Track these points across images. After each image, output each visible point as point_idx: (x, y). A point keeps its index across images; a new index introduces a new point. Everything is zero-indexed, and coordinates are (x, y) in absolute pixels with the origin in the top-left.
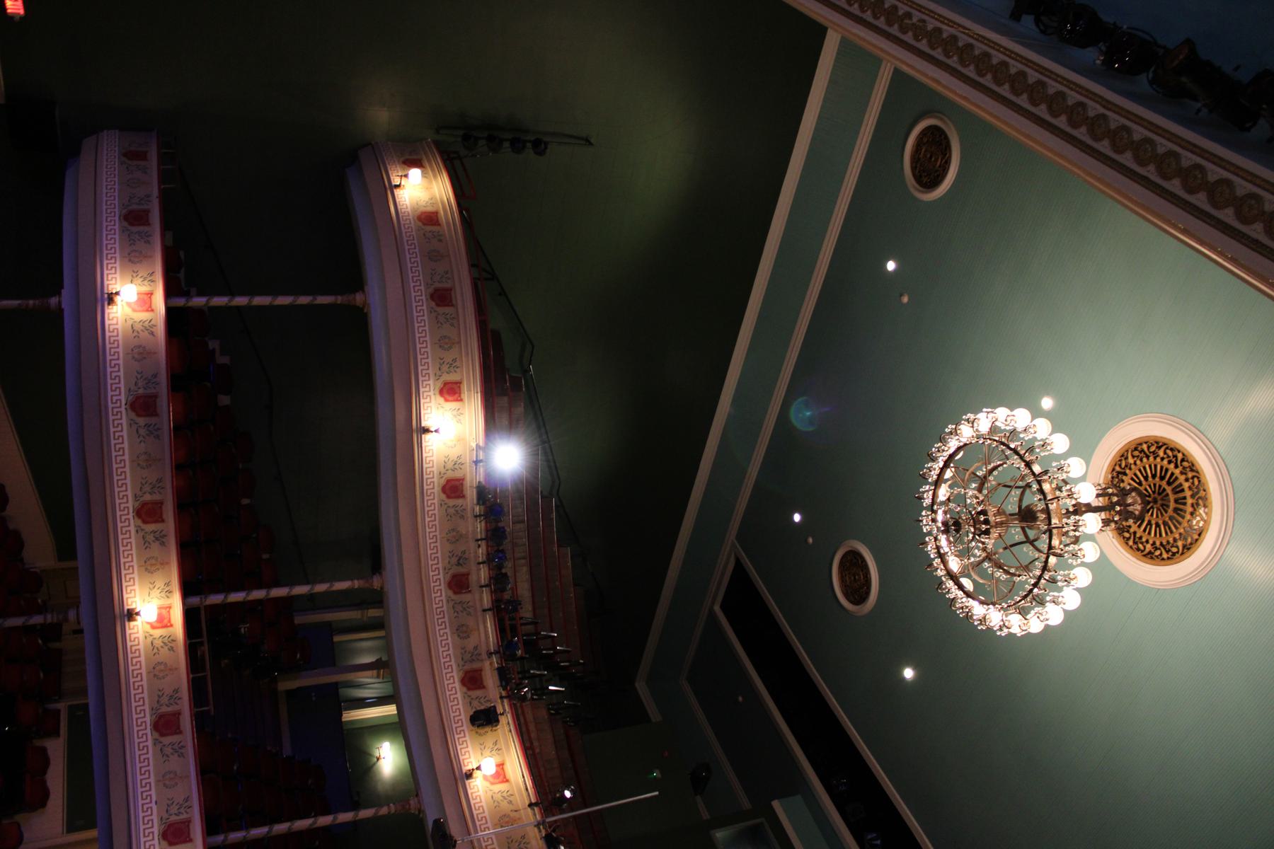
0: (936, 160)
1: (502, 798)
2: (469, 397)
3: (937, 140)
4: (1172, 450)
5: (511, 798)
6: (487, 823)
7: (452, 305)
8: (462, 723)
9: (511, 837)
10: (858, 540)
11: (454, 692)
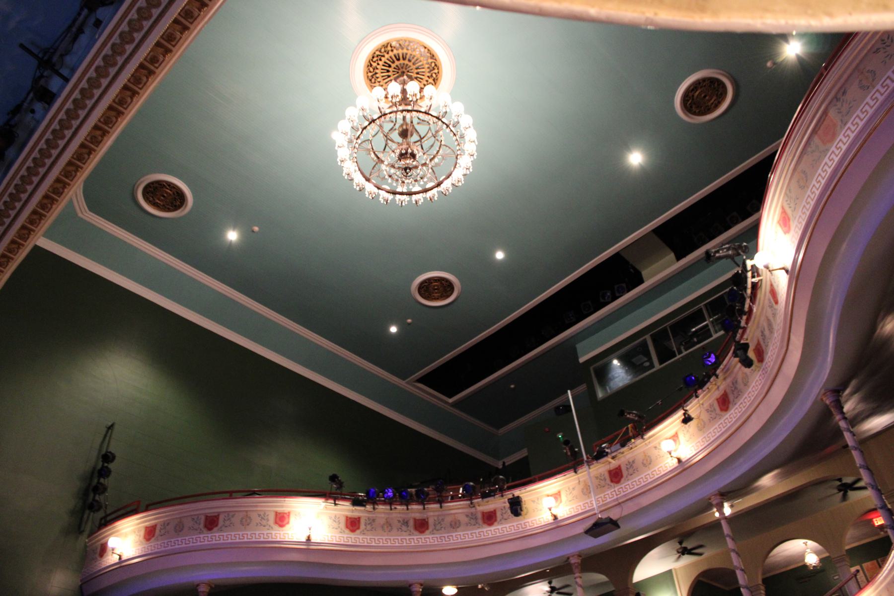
0: (167, 193)
1: (571, 495)
2: (288, 507)
3: (152, 189)
4: (373, 57)
5: (571, 488)
6: (587, 503)
7: (218, 515)
8: (519, 524)
9: (597, 486)
10: (410, 291)
11: (497, 530)
